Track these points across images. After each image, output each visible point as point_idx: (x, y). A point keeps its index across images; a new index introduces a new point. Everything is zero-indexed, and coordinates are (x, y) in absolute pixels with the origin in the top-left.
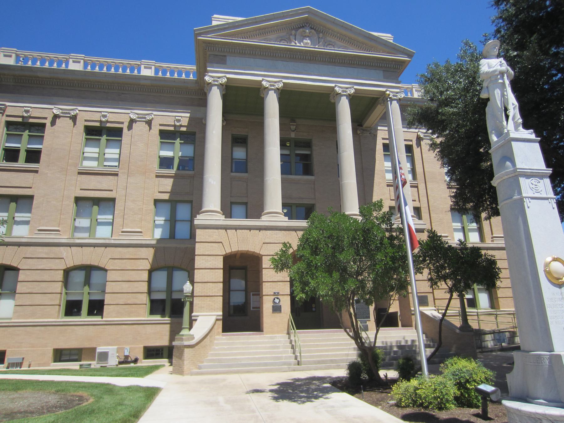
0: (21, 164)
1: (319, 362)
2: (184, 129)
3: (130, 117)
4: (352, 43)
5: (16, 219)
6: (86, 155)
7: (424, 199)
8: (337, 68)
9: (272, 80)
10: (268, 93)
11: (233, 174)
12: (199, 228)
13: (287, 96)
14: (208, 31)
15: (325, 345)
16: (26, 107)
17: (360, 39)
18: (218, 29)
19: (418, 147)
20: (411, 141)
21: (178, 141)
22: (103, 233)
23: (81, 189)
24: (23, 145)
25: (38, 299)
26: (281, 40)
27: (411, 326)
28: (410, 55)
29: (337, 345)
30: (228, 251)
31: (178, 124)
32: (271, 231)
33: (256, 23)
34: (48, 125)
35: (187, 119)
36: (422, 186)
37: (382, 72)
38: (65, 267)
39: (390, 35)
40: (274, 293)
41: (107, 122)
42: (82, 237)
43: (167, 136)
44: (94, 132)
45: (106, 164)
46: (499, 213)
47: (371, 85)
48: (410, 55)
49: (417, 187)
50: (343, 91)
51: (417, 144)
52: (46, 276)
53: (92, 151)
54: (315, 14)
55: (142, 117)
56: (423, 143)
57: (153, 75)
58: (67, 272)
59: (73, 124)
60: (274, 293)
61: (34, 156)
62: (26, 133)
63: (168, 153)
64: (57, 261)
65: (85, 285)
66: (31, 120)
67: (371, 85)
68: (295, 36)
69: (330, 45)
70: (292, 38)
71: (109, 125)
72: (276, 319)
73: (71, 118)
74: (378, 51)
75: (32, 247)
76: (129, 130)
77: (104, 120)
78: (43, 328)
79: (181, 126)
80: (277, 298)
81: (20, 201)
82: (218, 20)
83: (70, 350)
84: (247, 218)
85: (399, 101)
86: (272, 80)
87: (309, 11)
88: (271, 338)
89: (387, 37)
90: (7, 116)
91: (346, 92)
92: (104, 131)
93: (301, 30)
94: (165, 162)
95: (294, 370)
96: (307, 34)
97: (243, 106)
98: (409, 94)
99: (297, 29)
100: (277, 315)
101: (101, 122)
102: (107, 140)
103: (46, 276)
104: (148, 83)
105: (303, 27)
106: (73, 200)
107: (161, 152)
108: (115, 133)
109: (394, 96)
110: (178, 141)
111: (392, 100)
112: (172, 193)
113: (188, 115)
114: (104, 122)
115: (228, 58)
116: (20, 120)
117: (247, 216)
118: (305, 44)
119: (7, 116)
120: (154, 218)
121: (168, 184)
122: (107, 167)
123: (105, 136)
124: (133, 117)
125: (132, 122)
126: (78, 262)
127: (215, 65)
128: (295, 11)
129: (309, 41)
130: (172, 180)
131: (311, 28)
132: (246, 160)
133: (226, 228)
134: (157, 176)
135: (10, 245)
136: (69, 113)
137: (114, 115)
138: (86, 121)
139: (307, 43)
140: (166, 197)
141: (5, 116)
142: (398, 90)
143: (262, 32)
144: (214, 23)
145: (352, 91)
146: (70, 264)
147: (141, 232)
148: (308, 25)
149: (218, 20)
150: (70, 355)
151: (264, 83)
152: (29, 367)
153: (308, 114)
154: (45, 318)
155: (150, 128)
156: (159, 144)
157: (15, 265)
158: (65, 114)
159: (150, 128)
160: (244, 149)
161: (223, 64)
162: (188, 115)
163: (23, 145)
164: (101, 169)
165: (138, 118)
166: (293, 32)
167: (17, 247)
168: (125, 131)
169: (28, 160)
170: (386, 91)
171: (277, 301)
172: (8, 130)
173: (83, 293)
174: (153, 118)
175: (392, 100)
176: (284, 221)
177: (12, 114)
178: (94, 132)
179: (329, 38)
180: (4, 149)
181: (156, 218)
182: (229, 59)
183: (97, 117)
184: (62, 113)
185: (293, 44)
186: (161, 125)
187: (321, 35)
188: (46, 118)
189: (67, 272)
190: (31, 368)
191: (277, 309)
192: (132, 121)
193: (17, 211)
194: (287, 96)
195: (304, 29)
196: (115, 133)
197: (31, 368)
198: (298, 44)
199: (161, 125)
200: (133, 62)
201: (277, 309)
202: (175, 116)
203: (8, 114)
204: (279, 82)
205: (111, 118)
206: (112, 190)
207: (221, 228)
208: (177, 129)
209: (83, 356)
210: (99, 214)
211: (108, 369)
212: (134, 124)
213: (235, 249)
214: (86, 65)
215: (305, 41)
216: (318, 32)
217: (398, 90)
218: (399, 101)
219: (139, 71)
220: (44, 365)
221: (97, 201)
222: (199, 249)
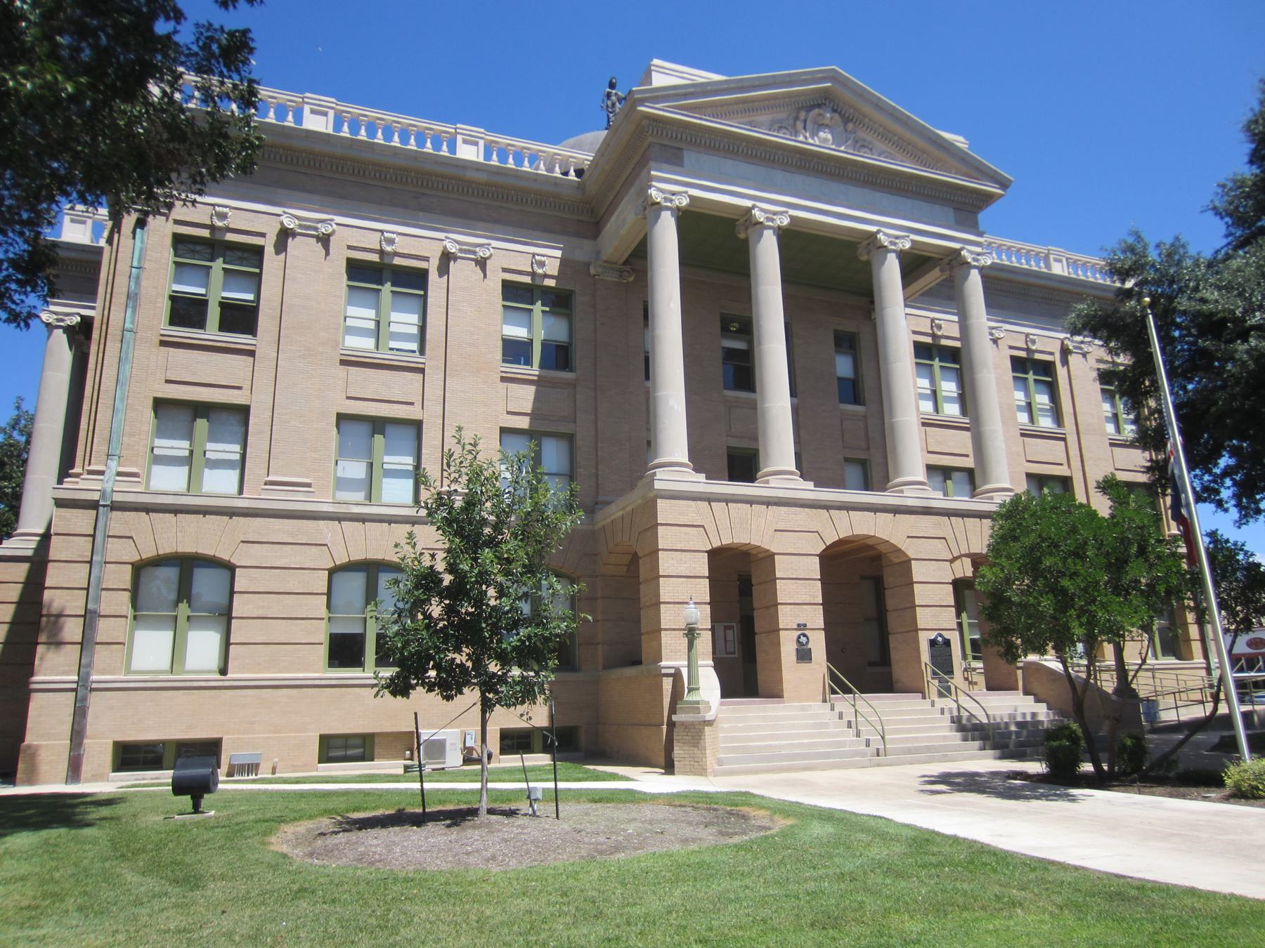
0: (211, 332)
1: (909, 751)
2: (551, 283)
3: (282, 223)
4: (904, 147)
5: (209, 455)
6: (350, 322)
7: (1076, 463)
8: (878, 195)
9: (772, 207)
10: (885, 258)
11: (729, 393)
12: (662, 497)
13: (795, 242)
14: (657, 97)
15: (903, 721)
16: (219, 206)
17: (922, 144)
18: (676, 95)
19: (441, 276)
20: (1052, 354)
21: (538, 307)
22: (220, 484)
23: (168, 381)
24: (217, 288)
25: (280, 631)
26: (780, 128)
27: (1016, 689)
28: (1004, 184)
29: (912, 722)
30: (716, 544)
31: (540, 271)
32: (786, 509)
33: (742, 89)
34: (269, 251)
35: (557, 262)
36: (1072, 439)
37: (952, 210)
38: (136, 558)
39: (961, 139)
40: (799, 625)
41: (396, 254)
42: (353, 500)
43: (517, 293)
44: (367, 274)
45: (393, 344)
46: (729, 456)
47: (938, 234)
48: (1004, 184)
49: (1064, 440)
50: (768, 219)
51: (439, 269)
52: (293, 582)
53: (362, 315)
54: (845, 83)
55: (469, 250)
56: (1071, 358)
57: (330, 131)
58: (139, 568)
59: (323, 252)
60: (799, 625)
61: (241, 318)
62: (218, 265)
63: (518, 332)
64: (314, 549)
65: (179, 600)
66: (230, 237)
67: (938, 234)
68: (805, 121)
69: (863, 146)
70: (800, 125)
71: (397, 261)
72: (804, 675)
73: (318, 239)
74: (947, 169)
75: (258, 519)
76: (278, 252)
77: (219, 224)
78: (295, 691)
79: (546, 276)
80: (805, 635)
81: (390, 430)
82: (666, 74)
83: (346, 737)
84: (866, 489)
85: (981, 269)
86: (772, 207)
87: (833, 77)
88: (803, 709)
89: (959, 141)
90: (177, 222)
91: (772, 220)
92: (386, 274)
93: (816, 111)
94: (515, 351)
95: (879, 765)
96: (827, 122)
97: (716, 249)
98: (445, 147)
99: (810, 108)
100: (804, 666)
101: (212, 228)
102: (1036, 380)
103: (293, 582)
104: (482, 177)
105: (819, 106)
106: (151, 402)
107: (349, 308)
108: (411, 280)
109: (768, 219)
110: (538, 307)
111: (887, 251)
112: (534, 416)
113: (558, 253)
114: (220, 229)
115: (686, 154)
116: (205, 233)
117: (867, 486)
118: (822, 142)
119: (177, 222)
120: (152, 441)
121: (525, 397)
122: (395, 352)
123: (221, 259)
124: (290, 224)
125: (285, 234)
126: (166, 548)
127: (666, 166)
128: (806, 70)
129: (829, 136)
130: (533, 388)
131: (834, 111)
132: (570, 344)
133: (710, 499)
134: (163, 344)
135: (211, 513)
136: (316, 229)
137: (414, 242)
138: (349, 247)
139: (826, 140)
140: (524, 423)
141: (170, 221)
142: (979, 250)
143: (748, 108)
144: (659, 80)
145: (908, 245)
146: (148, 552)
147: (309, 485)
148: (827, 104)
149: (666, 74)
150: (346, 747)
151: (756, 212)
152: (274, 773)
153: (833, 282)
154: (298, 671)
155: (327, 253)
156: (171, 266)
157: (226, 557)
158: (308, 230)
159: (327, 253)
160: (416, 304)
161: (676, 165)
162: (558, 253)
163: (217, 288)
164: (384, 356)
165: (461, 251)
166: (803, 115)
167: (226, 518)
168: (433, 276)
169: (224, 326)
170: (962, 249)
171: (803, 639)
172: (176, 255)
173: (176, 617)
174: (334, 232)
175: (887, 251)
176: (806, 489)
177: (188, 219)
178: (367, 274)
179: (862, 134)
180: (172, 298)
181: (158, 442)
182: (689, 157)
183: (372, 241)
184: (301, 226)
185: (801, 138)
186: (505, 270)
187: (850, 126)
188: (263, 235)
189: (139, 568)
190: (277, 775)
191: (804, 655)
192: (285, 234)
193: (213, 438)
194: (795, 242)
195: (821, 111)
196: (411, 280)
197: (277, 775)
198: (810, 141)
199: (505, 270)
200: (438, 127)
201: (804, 655)
202: (534, 255)
203: (178, 218)
204: (782, 213)
205: (401, 245)
206: (239, 388)
207: (700, 499)
208: (538, 282)
209: (377, 750)
210: (388, 453)
211: (449, 773)
212: (290, 240)
213: (726, 541)
214: (338, 125)
215: (821, 134)
216: (846, 120)
217: (979, 250)
218: (981, 269)
219: (452, 148)
220: (304, 767)
221: (378, 425)
222: (665, 537)
